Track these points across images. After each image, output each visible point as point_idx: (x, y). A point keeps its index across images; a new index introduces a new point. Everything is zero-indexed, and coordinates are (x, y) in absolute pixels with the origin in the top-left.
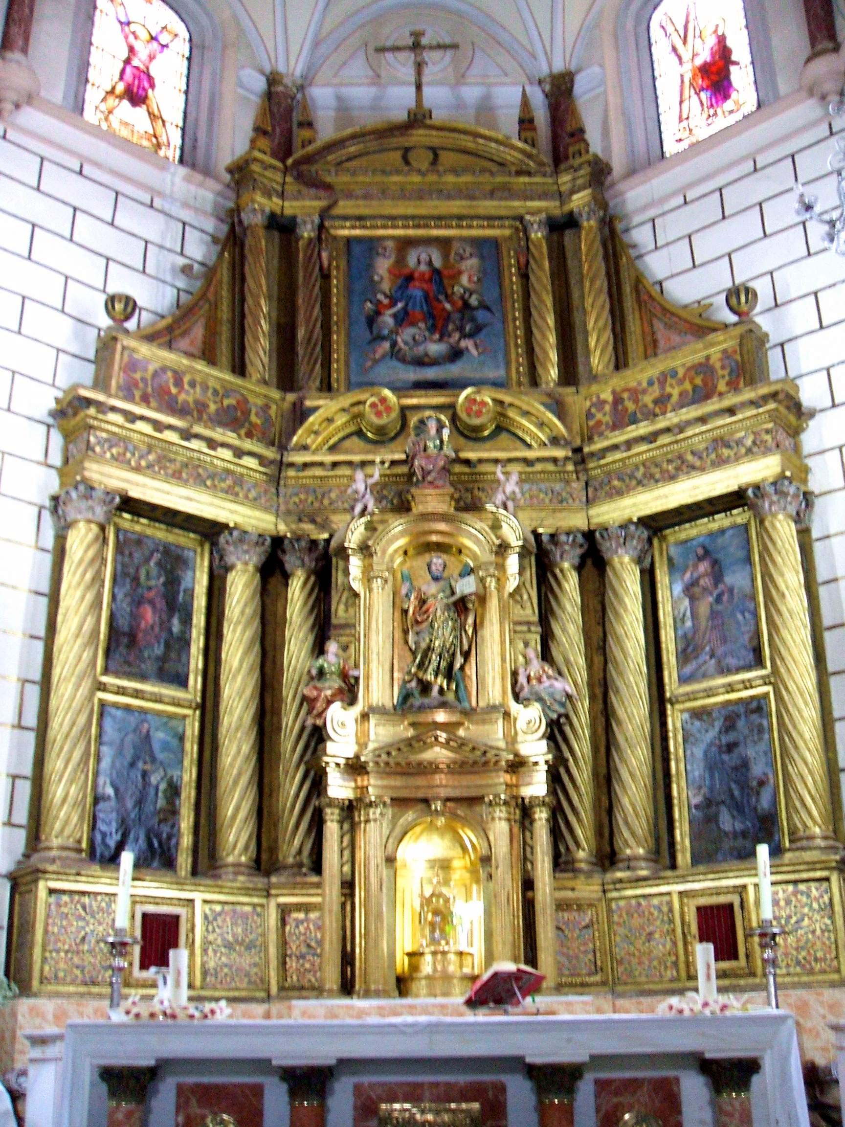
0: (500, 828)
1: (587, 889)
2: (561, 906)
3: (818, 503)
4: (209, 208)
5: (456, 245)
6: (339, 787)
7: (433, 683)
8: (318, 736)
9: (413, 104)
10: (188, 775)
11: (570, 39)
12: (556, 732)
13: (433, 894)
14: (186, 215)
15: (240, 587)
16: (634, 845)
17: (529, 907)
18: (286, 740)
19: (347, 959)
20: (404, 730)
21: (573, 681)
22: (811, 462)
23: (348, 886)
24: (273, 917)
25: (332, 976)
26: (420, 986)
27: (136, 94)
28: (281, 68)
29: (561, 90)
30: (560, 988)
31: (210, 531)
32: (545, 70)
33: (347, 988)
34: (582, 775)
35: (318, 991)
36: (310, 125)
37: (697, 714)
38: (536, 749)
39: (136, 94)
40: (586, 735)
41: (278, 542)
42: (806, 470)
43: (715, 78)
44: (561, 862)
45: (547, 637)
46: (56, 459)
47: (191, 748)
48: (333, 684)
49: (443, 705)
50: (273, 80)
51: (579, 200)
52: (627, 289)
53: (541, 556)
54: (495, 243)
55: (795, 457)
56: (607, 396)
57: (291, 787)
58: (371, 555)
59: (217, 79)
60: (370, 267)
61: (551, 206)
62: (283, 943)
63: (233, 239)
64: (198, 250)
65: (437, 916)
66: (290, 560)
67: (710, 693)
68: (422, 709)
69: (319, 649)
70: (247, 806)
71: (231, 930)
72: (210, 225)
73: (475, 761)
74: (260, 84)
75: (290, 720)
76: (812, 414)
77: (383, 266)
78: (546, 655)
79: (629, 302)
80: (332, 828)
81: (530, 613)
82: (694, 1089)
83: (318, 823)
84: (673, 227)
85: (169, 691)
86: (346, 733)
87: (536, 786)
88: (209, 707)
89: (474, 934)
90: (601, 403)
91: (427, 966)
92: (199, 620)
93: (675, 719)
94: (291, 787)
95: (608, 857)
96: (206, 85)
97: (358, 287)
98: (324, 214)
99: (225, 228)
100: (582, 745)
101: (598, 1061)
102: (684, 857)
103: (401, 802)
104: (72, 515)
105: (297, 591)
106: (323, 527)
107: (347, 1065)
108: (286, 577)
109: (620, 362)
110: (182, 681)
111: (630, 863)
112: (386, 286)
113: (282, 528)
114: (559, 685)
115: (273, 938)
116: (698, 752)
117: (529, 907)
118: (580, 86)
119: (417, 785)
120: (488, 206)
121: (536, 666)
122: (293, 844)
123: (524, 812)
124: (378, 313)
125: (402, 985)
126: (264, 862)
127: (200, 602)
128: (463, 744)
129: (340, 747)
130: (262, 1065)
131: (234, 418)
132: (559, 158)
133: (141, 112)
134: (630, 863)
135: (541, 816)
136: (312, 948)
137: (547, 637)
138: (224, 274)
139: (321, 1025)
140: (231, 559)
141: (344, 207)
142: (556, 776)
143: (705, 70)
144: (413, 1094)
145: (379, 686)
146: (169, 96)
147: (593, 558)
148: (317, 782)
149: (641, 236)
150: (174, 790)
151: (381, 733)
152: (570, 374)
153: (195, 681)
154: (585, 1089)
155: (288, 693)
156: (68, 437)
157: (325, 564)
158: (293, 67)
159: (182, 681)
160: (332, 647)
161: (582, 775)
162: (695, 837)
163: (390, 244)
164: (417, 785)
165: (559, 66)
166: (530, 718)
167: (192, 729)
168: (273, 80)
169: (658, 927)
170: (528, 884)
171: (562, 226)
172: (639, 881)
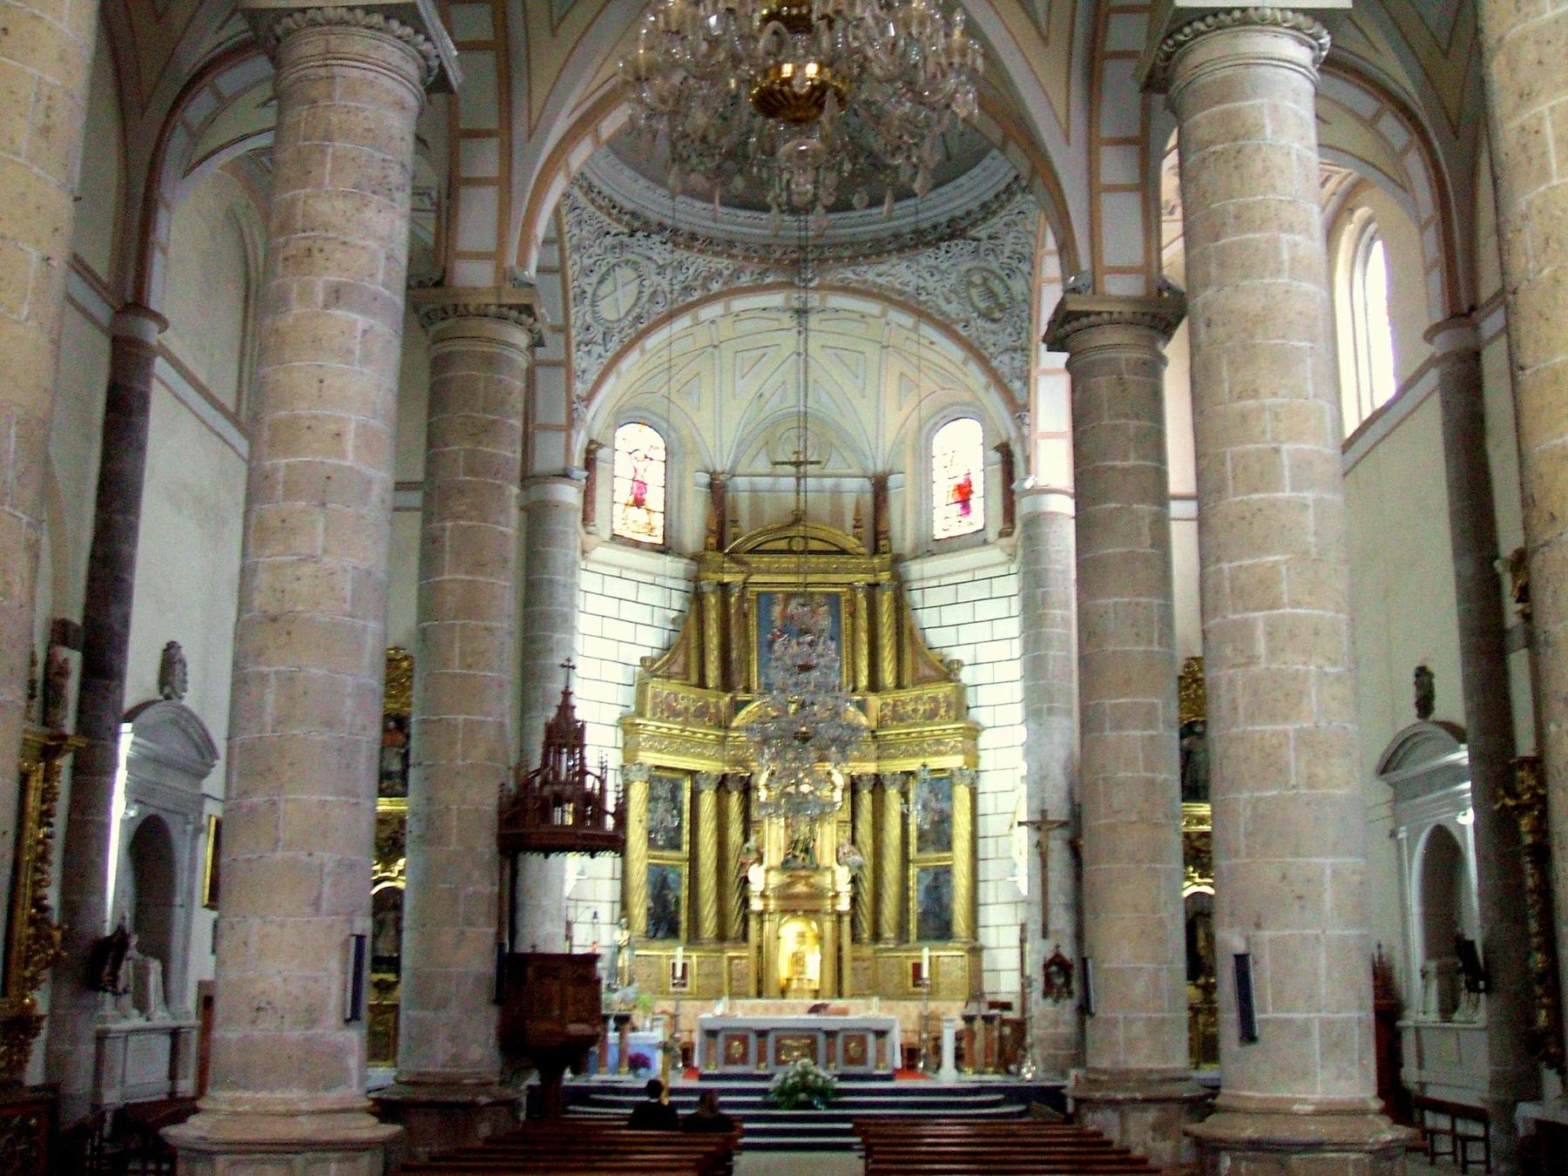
0: (828, 925)
2: (855, 959)
3: (983, 775)
7: (800, 855)
8: (746, 880)
10: (684, 893)
11: (888, 449)
13: (797, 948)
15: (708, 800)
16: (889, 932)
17: (839, 959)
18: (733, 884)
19: (759, 981)
21: (864, 858)
22: (981, 753)
23: (760, 948)
24: (725, 963)
25: (752, 989)
27: (639, 503)
30: (852, 996)
31: (692, 773)
33: (759, 994)
34: (866, 898)
35: (747, 996)
36: (735, 522)
37: (924, 870)
38: (845, 888)
39: (639, 503)
40: (867, 885)
41: (725, 776)
42: (978, 757)
44: (855, 939)
46: (620, 744)
47: (685, 881)
48: (754, 856)
51: (884, 577)
52: (906, 632)
54: (837, 595)
55: (973, 756)
56: (890, 701)
57: (734, 902)
59: (682, 477)
60: (769, 611)
61: (870, 578)
62: (730, 974)
63: (697, 598)
64: (677, 602)
65: (798, 960)
66: (730, 785)
67: (928, 860)
69: (746, 840)
70: (714, 910)
71: (706, 969)
72: (682, 585)
73: (817, 894)
75: (732, 865)
76: (984, 729)
78: (853, 841)
79: (906, 641)
80: (753, 924)
82: (871, 1038)
85: (674, 854)
87: (844, 905)
88: (693, 859)
89: (814, 968)
90: (886, 704)
91: (794, 985)
92: (686, 816)
93: (913, 871)
94: (734, 902)
95: (877, 936)
96: (675, 481)
97: (765, 623)
98: (745, 584)
101: (843, 1030)
102: (913, 937)
103: (784, 912)
105: (734, 800)
108: (729, 793)
109: (899, 685)
110: (678, 847)
112: (778, 623)
113: (727, 769)
114: (858, 858)
116: (922, 888)
117: (839, 959)
121: (847, 848)
122: (734, 928)
123: (840, 915)
125: (783, 993)
126: (721, 936)
127: (687, 807)
128: (812, 886)
130: (749, 1029)
131: (701, 713)
132: (876, 551)
133: (642, 511)
135: (847, 919)
136: (744, 976)
138: (692, 620)
139: (750, 1012)
140: (702, 787)
142: (854, 900)
143: (960, 488)
144: (791, 1037)
145: (774, 856)
146: (655, 498)
148: (746, 902)
151: (775, 879)
152: (875, 686)
153: (686, 847)
156: (625, 733)
157: (747, 788)
158: (722, 464)
159: (678, 847)
160: (753, 838)
161: (866, 898)
165: (880, 468)
166: (843, 877)
167: (685, 870)
168: (713, 475)
170: (839, 949)
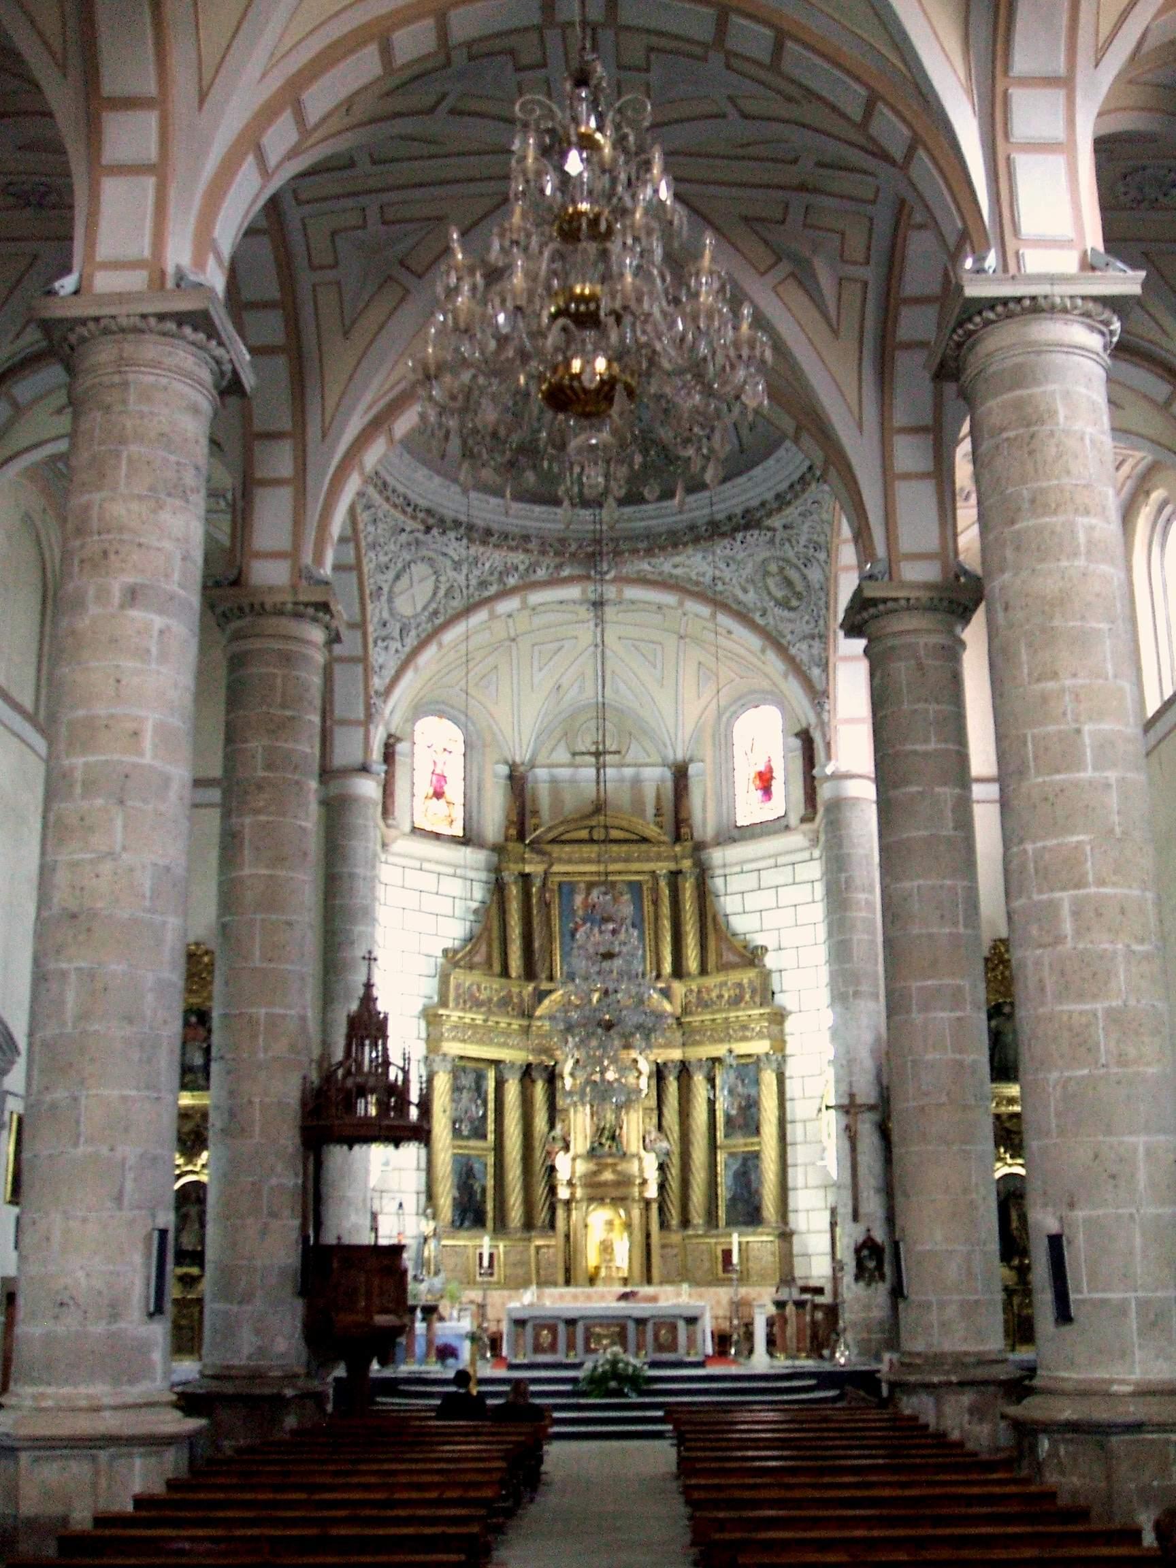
0: (636, 1212)
1: (675, 1238)
2: (663, 1246)
4: (483, 865)
5: (619, 886)
6: (563, 1193)
7: (607, 1141)
8: (552, 1169)
9: (594, 794)
10: (490, 1183)
11: (687, 738)
12: (662, 1167)
13: (604, 1235)
14: (472, 874)
15: (512, 1090)
16: (698, 1218)
18: (538, 1171)
19: (567, 1270)
20: (592, 1166)
21: (670, 1144)
23: (567, 1236)
24: (533, 1251)
25: (561, 1278)
26: (599, 1282)
27: (438, 795)
28: (518, 760)
29: (681, 775)
30: (661, 1283)
31: (496, 1063)
32: (671, 757)
35: (555, 1284)
38: (652, 1175)
40: (676, 1171)
41: (529, 1066)
43: (765, 781)
44: (664, 1225)
45: (660, 1116)
46: (424, 1035)
47: (491, 1170)
49: (611, 1155)
50: (513, 767)
52: (710, 919)
53: (659, 1074)
54: (639, 883)
55: (779, 1044)
56: (694, 987)
57: (541, 1190)
58: (602, 1243)
59: (481, 769)
60: (571, 901)
63: (498, 888)
64: (479, 893)
65: (606, 1248)
66: (534, 1074)
68: (601, 1157)
69: (552, 1125)
71: (514, 1258)
74: (504, 770)
75: (538, 1154)
77: (579, 899)
78: (660, 1127)
80: (560, 1213)
81: (653, 1103)
83: (552, 1209)
84: (735, 883)
86: (564, 1165)
88: (499, 1148)
89: (623, 1255)
91: (603, 1273)
94: (541, 1190)
96: (475, 773)
99: (493, 876)
100: (674, 1171)
104: (435, 1068)
105: (539, 1090)
106: (551, 1057)
107: (582, 1318)
108: (533, 1081)
109: (703, 971)
111: (695, 1227)
112: (580, 913)
113: (531, 1058)
115: (533, 1259)
116: (731, 1173)
117: (648, 1246)
118: (692, 769)
119: (599, 1192)
120: (635, 866)
121: (654, 1134)
122: (542, 1216)
123: (648, 1203)
124: (576, 930)
127: (491, 1096)
129: (563, 1175)
130: (558, 1318)
131: (505, 1002)
132: (678, 838)
134: (695, 1227)
135: (655, 1206)
136: (551, 1264)
137: (660, 1116)
138: (494, 911)
141: (555, 868)
142: (662, 1187)
143: (760, 775)
144: (601, 1325)
145: (580, 1144)
146: (455, 790)
147: (684, 1070)
148: (552, 1190)
149: (719, 883)
150: (484, 1190)
152: (679, 972)
153: (491, 1137)
154: (650, 1327)
155: (537, 1144)
156: (429, 1024)
157: (552, 1077)
158: (521, 755)
159: (484, 1137)
161: (674, 1184)
162: (728, 1212)
163: (582, 886)
164: (599, 1192)
167: (491, 1160)
168: (513, 767)
169: (705, 1257)
170: (648, 1236)
171: (675, 875)
172: (698, 1236)
